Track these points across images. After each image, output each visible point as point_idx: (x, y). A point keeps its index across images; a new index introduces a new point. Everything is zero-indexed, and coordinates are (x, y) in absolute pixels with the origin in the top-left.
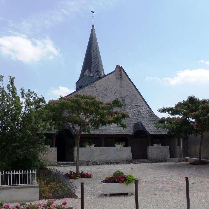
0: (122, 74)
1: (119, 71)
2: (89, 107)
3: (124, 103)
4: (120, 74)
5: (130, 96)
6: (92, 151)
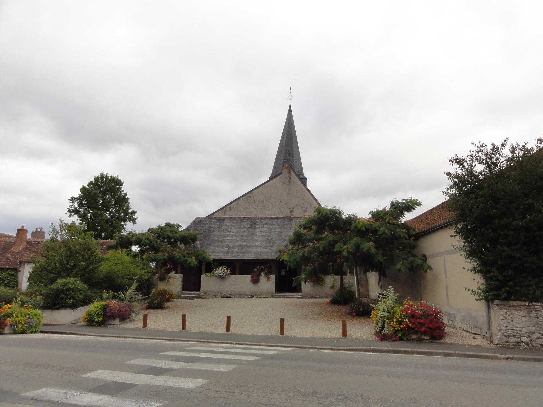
0: (292, 176)
1: (287, 173)
2: (536, 196)
3: (293, 215)
4: (289, 177)
5: (303, 206)
6: (46, 270)
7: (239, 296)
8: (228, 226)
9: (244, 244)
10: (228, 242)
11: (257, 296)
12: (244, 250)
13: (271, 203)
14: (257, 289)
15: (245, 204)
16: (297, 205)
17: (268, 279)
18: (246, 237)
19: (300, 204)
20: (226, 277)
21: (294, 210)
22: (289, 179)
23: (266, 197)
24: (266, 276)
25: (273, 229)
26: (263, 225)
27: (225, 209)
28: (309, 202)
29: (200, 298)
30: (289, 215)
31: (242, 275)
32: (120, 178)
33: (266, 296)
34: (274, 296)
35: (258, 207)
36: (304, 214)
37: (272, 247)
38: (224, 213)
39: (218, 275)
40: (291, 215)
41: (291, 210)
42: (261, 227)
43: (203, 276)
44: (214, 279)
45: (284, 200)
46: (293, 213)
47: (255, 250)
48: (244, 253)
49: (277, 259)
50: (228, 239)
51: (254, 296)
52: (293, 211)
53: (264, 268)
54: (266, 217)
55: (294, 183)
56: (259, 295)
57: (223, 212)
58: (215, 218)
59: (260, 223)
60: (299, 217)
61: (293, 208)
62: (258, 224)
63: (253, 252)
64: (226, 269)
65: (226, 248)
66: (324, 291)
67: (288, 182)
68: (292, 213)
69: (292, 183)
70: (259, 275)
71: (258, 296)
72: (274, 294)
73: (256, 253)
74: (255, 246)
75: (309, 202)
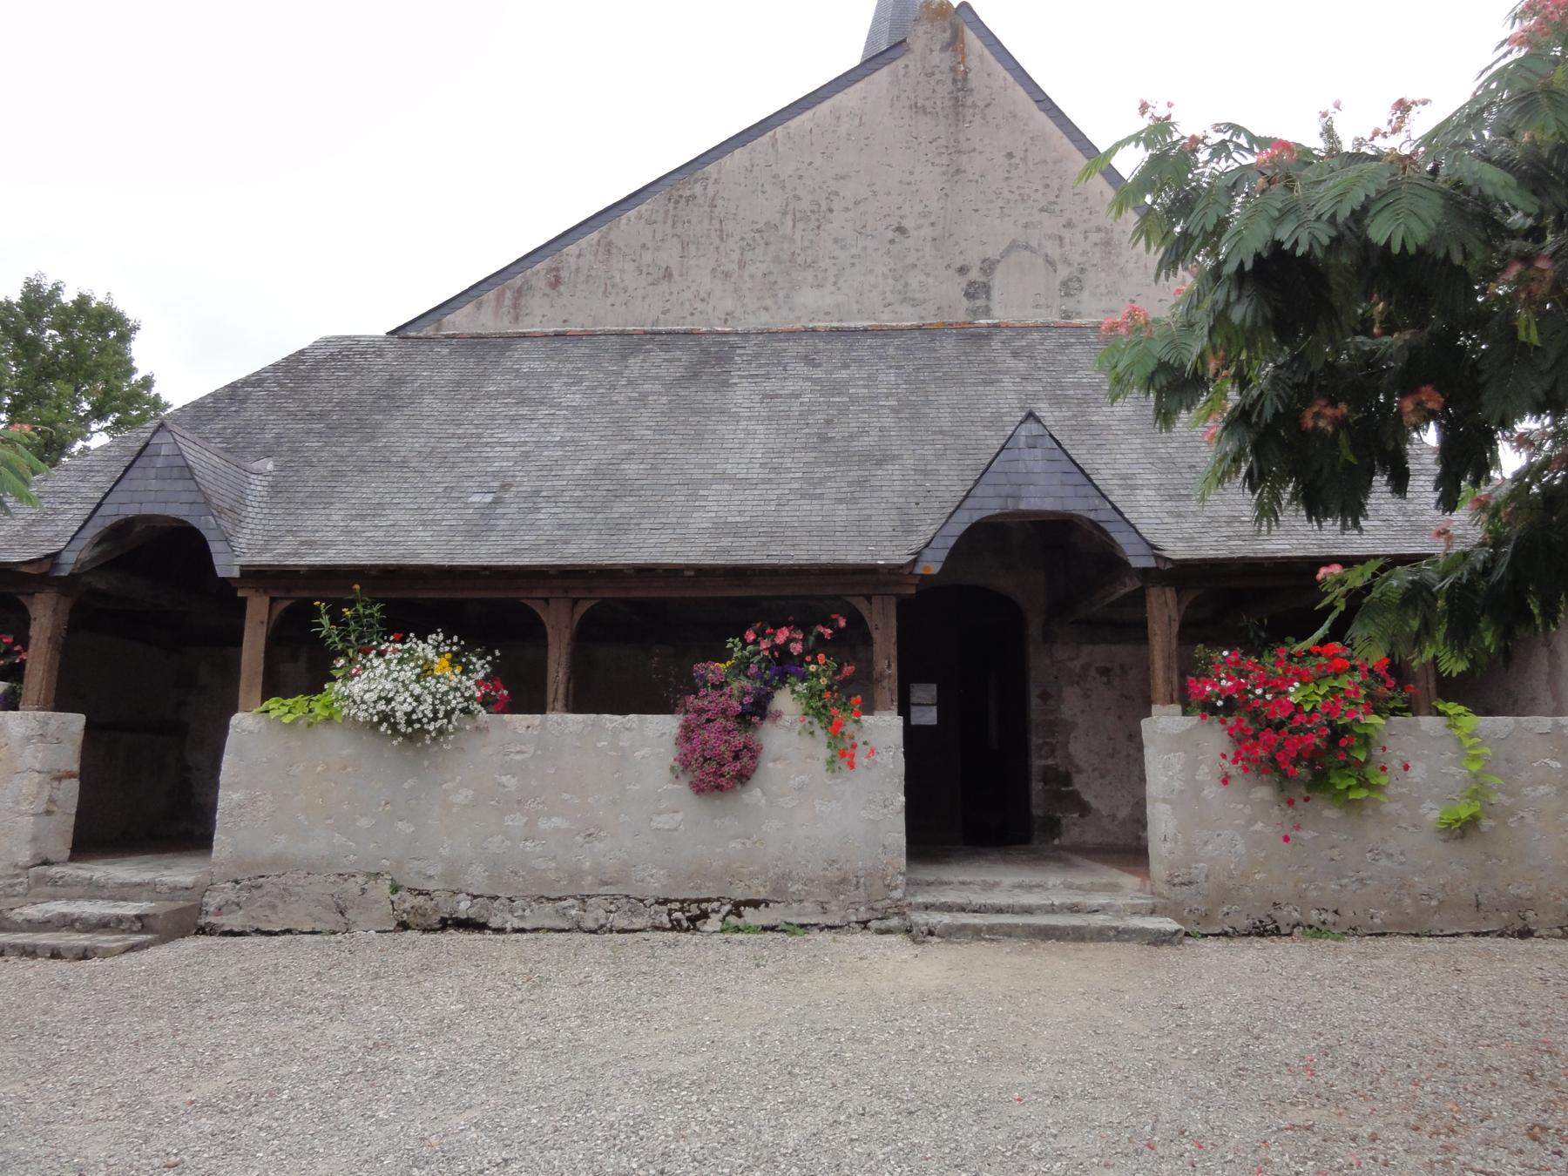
0: (973, 62)
4: (953, 69)
5: (1052, 249)
7: (563, 914)
8: (528, 376)
9: (632, 469)
10: (508, 459)
11: (737, 908)
12: (621, 508)
13: (836, 241)
14: (735, 845)
15: (657, 249)
16: (1013, 246)
17: (844, 755)
18: (649, 427)
19: (1034, 244)
20: (441, 731)
21: (998, 281)
22: (955, 81)
23: (798, 198)
24: (817, 726)
25: (855, 386)
26: (779, 363)
27: (518, 280)
28: (1099, 230)
29: (202, 931)
30: (960, 316)
31: (598, 712)
32: (121, 305)
33: (825, 912)
34: (901, 914)
35: (742, 265)
36: (1069, 304)
37: (862, 483)
38: (515, 305)
39: (362, 716)
40: (975, 312)
41: (970, 284)
42: (767, 377)
43: (242, 723)
44: (338, 747)
45: (923, 215)
46: (988, 298)
47: (715, 506)
48: (619, 527)
49: (919, 570)
50: (514, 445)
51: (705, 915)
52: (986, 289)
53: (796, 648)
54: (798, 326)
55: (988, 105)
56: (755, 904)
57: (508, 302)
58: (447, 337)
59: (757, 356)
60: (1030, 322)
61: (989, 266)
62: (749, 362)
63: (701, 520)
64: (454, 662)
65: (475, 498)
66: (1384, 862)
67: (948, 103)
68: (980, 302)
69: (974, 106)
70: (757, 710)
71: (748, 912)
72: (897, 894)
73: (721, 528)
74: (723, 478)
75: (1099, 230)
